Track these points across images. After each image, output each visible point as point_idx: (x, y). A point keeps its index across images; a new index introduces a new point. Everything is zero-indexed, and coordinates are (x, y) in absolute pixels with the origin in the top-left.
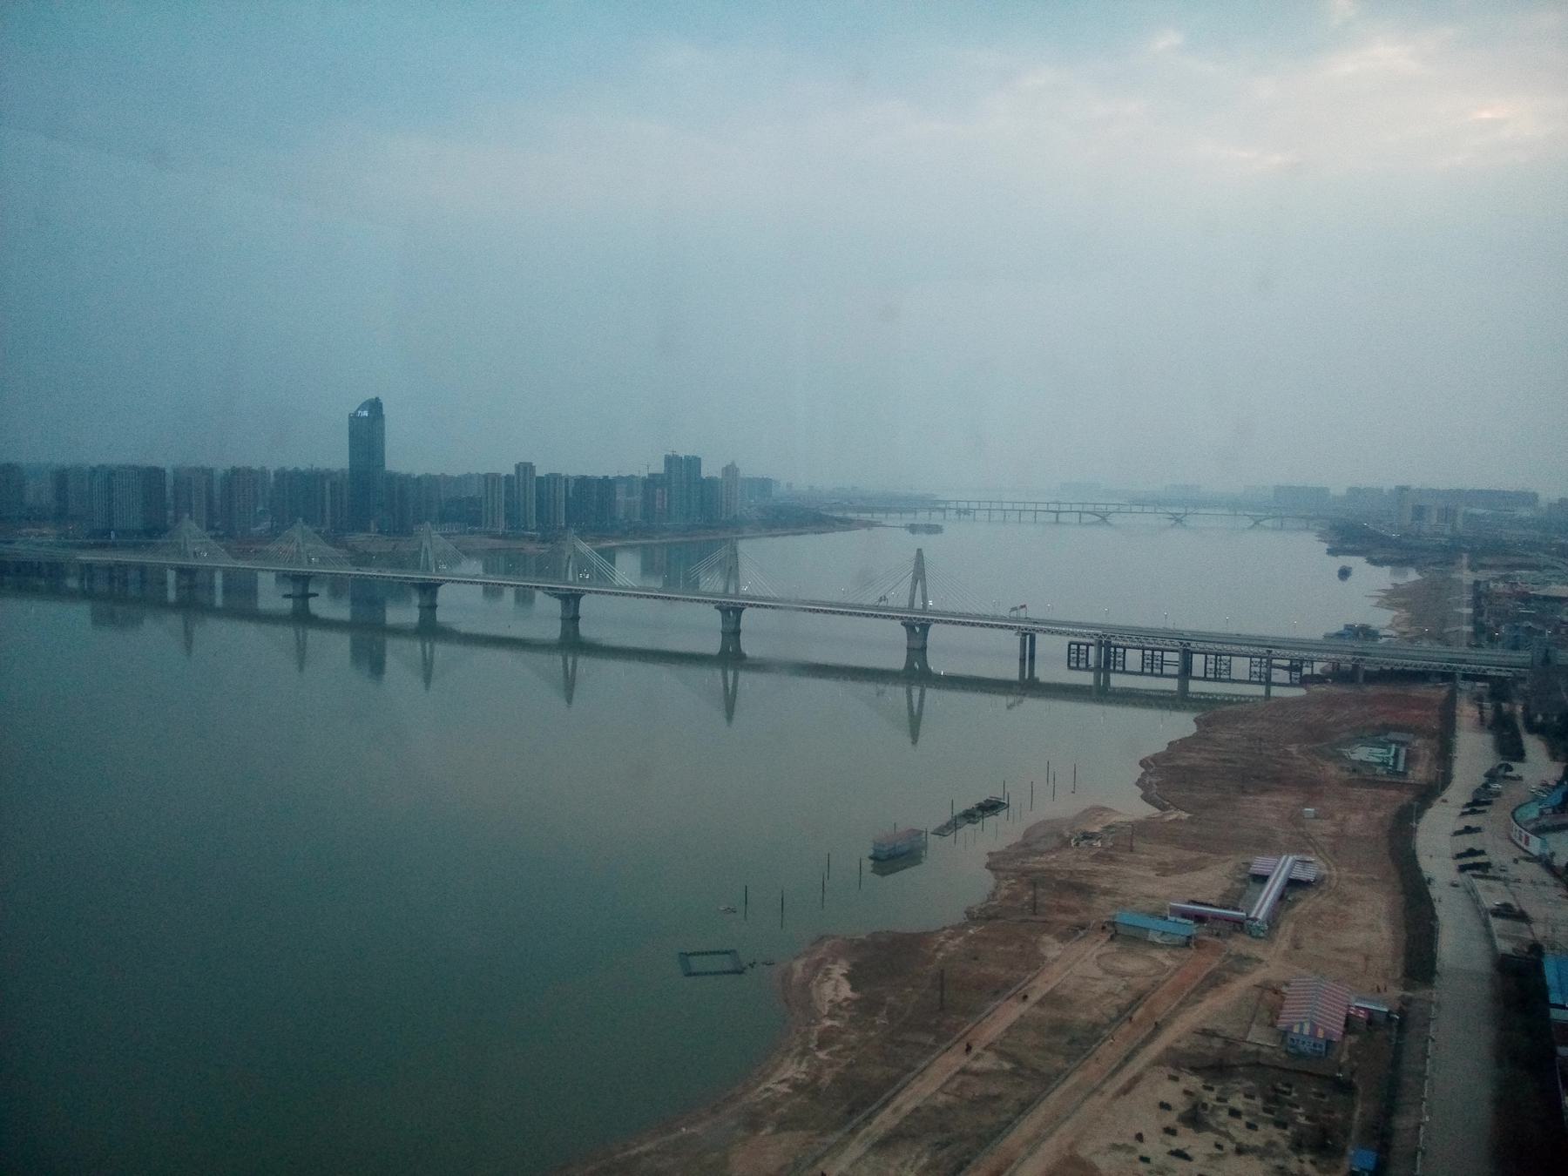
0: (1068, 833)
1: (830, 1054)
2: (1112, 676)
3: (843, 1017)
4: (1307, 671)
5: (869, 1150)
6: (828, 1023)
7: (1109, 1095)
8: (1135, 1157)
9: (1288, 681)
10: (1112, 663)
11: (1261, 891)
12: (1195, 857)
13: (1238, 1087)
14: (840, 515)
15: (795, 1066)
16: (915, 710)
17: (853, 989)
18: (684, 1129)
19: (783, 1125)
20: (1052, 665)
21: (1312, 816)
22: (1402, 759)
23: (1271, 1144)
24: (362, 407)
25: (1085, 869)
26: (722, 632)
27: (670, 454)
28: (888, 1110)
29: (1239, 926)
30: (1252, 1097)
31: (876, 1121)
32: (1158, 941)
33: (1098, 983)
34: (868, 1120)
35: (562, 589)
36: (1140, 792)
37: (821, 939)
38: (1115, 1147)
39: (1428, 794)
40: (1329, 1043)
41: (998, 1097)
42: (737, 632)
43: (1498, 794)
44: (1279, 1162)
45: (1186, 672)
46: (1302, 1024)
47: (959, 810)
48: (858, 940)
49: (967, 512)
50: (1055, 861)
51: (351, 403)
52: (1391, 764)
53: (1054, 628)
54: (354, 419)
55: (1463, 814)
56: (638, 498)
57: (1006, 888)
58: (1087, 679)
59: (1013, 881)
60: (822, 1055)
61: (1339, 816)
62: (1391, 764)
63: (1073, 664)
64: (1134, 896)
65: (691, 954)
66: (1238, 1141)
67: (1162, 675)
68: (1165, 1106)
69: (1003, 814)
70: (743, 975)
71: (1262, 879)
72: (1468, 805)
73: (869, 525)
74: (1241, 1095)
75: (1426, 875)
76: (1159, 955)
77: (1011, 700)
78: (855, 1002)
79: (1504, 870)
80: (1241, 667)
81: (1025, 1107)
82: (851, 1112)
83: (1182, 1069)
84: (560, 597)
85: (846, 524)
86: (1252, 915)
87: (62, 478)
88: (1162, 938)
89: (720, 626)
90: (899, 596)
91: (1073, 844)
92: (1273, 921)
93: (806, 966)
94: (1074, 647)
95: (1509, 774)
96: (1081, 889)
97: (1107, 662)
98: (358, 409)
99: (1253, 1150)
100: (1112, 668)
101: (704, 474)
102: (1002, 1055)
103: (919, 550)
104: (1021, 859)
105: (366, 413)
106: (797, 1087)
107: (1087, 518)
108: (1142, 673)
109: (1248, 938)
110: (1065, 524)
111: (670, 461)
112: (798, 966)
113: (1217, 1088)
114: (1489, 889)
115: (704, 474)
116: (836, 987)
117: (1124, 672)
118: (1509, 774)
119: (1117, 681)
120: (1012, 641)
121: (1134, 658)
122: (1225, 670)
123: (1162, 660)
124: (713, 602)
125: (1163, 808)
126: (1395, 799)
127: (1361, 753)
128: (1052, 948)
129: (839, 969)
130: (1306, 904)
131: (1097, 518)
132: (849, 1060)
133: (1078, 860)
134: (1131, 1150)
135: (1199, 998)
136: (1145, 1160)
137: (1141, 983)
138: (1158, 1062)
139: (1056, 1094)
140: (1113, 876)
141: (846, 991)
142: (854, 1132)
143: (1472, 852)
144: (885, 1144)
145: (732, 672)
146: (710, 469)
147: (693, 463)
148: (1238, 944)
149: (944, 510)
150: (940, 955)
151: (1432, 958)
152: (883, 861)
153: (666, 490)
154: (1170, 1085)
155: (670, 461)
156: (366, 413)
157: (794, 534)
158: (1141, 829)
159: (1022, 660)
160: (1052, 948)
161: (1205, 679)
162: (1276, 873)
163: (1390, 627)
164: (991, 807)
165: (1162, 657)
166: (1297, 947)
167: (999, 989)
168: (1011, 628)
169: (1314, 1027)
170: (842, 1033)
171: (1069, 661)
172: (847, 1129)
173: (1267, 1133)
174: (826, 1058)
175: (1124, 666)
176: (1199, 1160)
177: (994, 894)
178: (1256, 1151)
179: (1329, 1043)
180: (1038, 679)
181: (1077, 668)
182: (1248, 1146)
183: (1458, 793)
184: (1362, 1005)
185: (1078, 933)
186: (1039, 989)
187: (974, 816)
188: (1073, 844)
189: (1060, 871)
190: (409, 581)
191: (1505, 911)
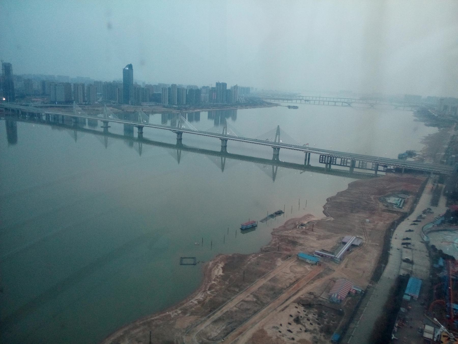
0: (298, 223)
1: (210, 292)
2: (332, 165)
3: (217, 281)
4: (389, 168)
5: (211, 323)
6: (213, 282)
7: (278, 311)
8: (277, 331)
9: (383, 170)
10: (332, 161)
11: (344, 246)
12: (330, 234)
13: (313, 311)
14: (268, 101)
15: (201, 295)
17: (223, 272)
18: (167, 313)
19: (192, 314)
20: (315, 161)
21: (368, 222)
22: (402, 203)
23: (315, 329)
24: (127, 67)
25: (298, 236)
26: (221, 146)
28: (220, 311)
29: (332, 259)
30: (315, 315)
31: (215, 314)
33: (288, 275)
34: (214, 314)
35: (177, 131)
36: (323, 209)
37: (219, 255)
38: (274, 327)
39: (404, 216)
40: (341, 301)
41: (248, 310)
42: (226, 146)
43: (424, 218)
44: (315, 335)
45: (353, 166)
46: (335, 294)
47: (270, 214)
48: (229, 256)
49: (308, 101)
50: (290, 233)
52: (398, 205)
54: (124, 70)
55: (412, 224)
56: (208, 95)
57: (274, 241)
58: (323, 166)
59: (277, 239)
60: (209, 292)
61: (376, 222)
62: (398, 205)
63: (321, 161)
64: (308, 246)
65: (184, 258)
66: (306, 328)
67: (346, 166)
68: (291, 316)
69: (282, 215)
70: (195, 266)
71: (344, 243)
72: (414, 221)
73: (277, 105)
74: (312, 314)
75: (392, 245)
76: (307, 267)
77: (302, 171)
78: (222, 276)
79: (414, 246)
80: (370, 165)
81: (255, 312)
82: (210, 311)
83: (300, 305)
84: (177, 133)
85: (270, 105)
86: (336, 257)
87: (43, 84)
88: (310, 262)
89: (221, 145)
91: (298, 227)
92: (341, 259)
93: (212, 264)
94: (322, 156)
95: (430, 211)
96: (294, 243)
97: (330, 162)
98: (126, 67)
99: (310, 331)
100: (332, 163)
102: (255, 296)
103: (278, 126)
104: (281, 232)
105: (128, 69)
106: (199, 302)
107: (344, 104)
108: (341, 165)
109: (334, 263)
110: (337, 106)
111: (218, 84)
112: (211, 263)
113: (307, 311)
114: (407, 252)
116: (218, 272)
117: (335, 164)
118: (430, 211)
119: (333, 167)
120: (303, 154)
121: (338, 161)
122: (365, 166)
123: (347, 162)
124: (219, 138)
125: (327, 216)
126: (396, 217)
127: (392, 200)
128: (279, 262)
129: (221, 265)
130: (355, 252)
131: (347, 104)
132: (215, 295)
133: (297, 233)
134: (278, 328)
135: (313, 282)
136: (280, 332)
137: (299, 276)
138: (294, 302)
139: (265, 309)
140: (304, 239)
141: (221, 273)
142: (209, 317)
143: (407, 239)
144: (215, 322)
147: (224, 85)
148: (330, 265)
149: (301, 100)
150: (249, 263)
151: (381, 274)
152: (243, 230)
153: (216, 93)
154: (295, 309)
155: (218, 84)
156: (128, 69)
157: (253, 108)
158: (319, 223)
159: (306, 160)
160: (279, 262)
161: (359, 168)
162: (349, 242)
163: (421, 151)
164: (279, 213)
165: (347, 161)
166: (346, 267)
167: (262, 275)
168: (303, 151)
169: (338, 295)
170: (216, 286)
171: (320, 161)
172: (207, 316)
173: (316, 326)
174: (209, 293)
175: (336, 163)
176: (295, 332)
177: (270, 243)
178: (310, 331)
179: (341, 301)
180: (310, 165)
181: (322, 163)
182: (308, 329)
183: (413, 217)
184: (354, 289)
185: (288, 258)
186: (272, 275)
187: (273, 216)
188: (298, 227)
189: (290, 236)
191: (407, 261)
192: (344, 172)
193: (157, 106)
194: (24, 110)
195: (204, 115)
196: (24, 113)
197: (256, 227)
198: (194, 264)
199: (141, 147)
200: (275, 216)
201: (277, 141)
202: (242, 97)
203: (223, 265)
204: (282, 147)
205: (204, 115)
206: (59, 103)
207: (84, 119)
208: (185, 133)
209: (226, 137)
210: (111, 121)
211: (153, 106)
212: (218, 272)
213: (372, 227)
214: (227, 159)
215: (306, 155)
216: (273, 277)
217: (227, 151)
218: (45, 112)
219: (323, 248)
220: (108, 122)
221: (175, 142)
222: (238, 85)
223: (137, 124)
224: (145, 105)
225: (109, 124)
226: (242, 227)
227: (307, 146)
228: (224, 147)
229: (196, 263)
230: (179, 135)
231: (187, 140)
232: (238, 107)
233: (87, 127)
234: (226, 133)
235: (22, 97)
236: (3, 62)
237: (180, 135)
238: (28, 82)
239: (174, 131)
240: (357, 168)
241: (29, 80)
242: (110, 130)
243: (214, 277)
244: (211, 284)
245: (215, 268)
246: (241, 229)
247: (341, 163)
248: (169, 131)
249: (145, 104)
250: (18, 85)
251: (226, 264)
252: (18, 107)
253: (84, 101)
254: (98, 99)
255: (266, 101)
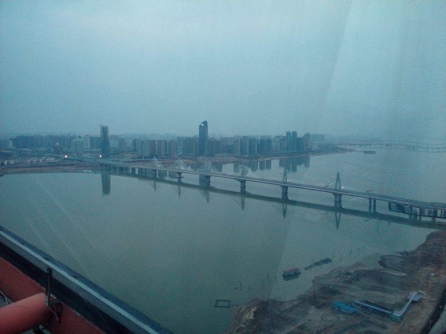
6: (242, 325)
16: (285, 208)
17: (254, 316)
24: (202, 123)
27: (288, 131)
32: (344, 311)
35: (241, 179)
42: (340, 201)
45: (435, 216)
49: (389, 145)
51: (200, 122)
53: (383, 197)
54: (200, 126)
76: (341, 316)
77: (366, 218)
84: (240, 181)
85: (344, 150)
87: (135, 142)
90: (332, 185)
103: (338, 173)
105: (203, 125)
111: (288, 133)
112: (244, 307)
120: (280, 189)
133: (339, 282)
141: (251, 317)
145: (285, 205)
146: (300, 134)
147: (295, 133)
156: (203, 125)
159: (370, 207)
161: (441, 217)
164: (327, 261)
170: (244, 329)
190: (203, 175)
192: (442, 223)
193: (229, 156)
194: (115, 165)
195: (275, 163)
196: (115, 168)
197: (299, 275)
198: (228, 307)
199: (340, 219)
200: (321, 264)
201: (338, 188)
202: (316, 144)
203: (256, 309)
204: (289, 186)
205: (275, 163)
206: (145, 158)
207: (166, 172)
208: (248, 181)
209: (286, 184)
210: (183, 172)
211: (225, 156)
212: (249, 316)
213: (437, 281)
214: (288, 205)
215: (370, 202)
216: (302, 324)
217: (288, 197)
218: (131, 166)
219: (367, 299)
220: (181, 173)
221: (239, 190)
222: (310, 134)
223: (205, 174)
224: (218, 156)
225: (183, 175)
226: (284, 273)
227: (371, 192)
228: (285, 194)
229: (230, 306)
230: (242, 182)
231: (250, 188)
232: (309, 155)
233: (167, 178)
234: (286, 180)
235: (117, 153)
236: (102, 126)
237: (243, 183)
238: (122, 141)
239: (237, 180)
240: (439, 217)
241: (123, 139)
242: (183, 180)
243: (243, 321)
244: (239, 327)
245: (247, 312)
246: (283, 276)
247: (441, 215)
248: (233, 179)
249: (218, 155)
250: (113, 144)
251: (258, 309)
252: (111, 162)
253: (165, 155)
254: (179, 153)
255: (340, 146)
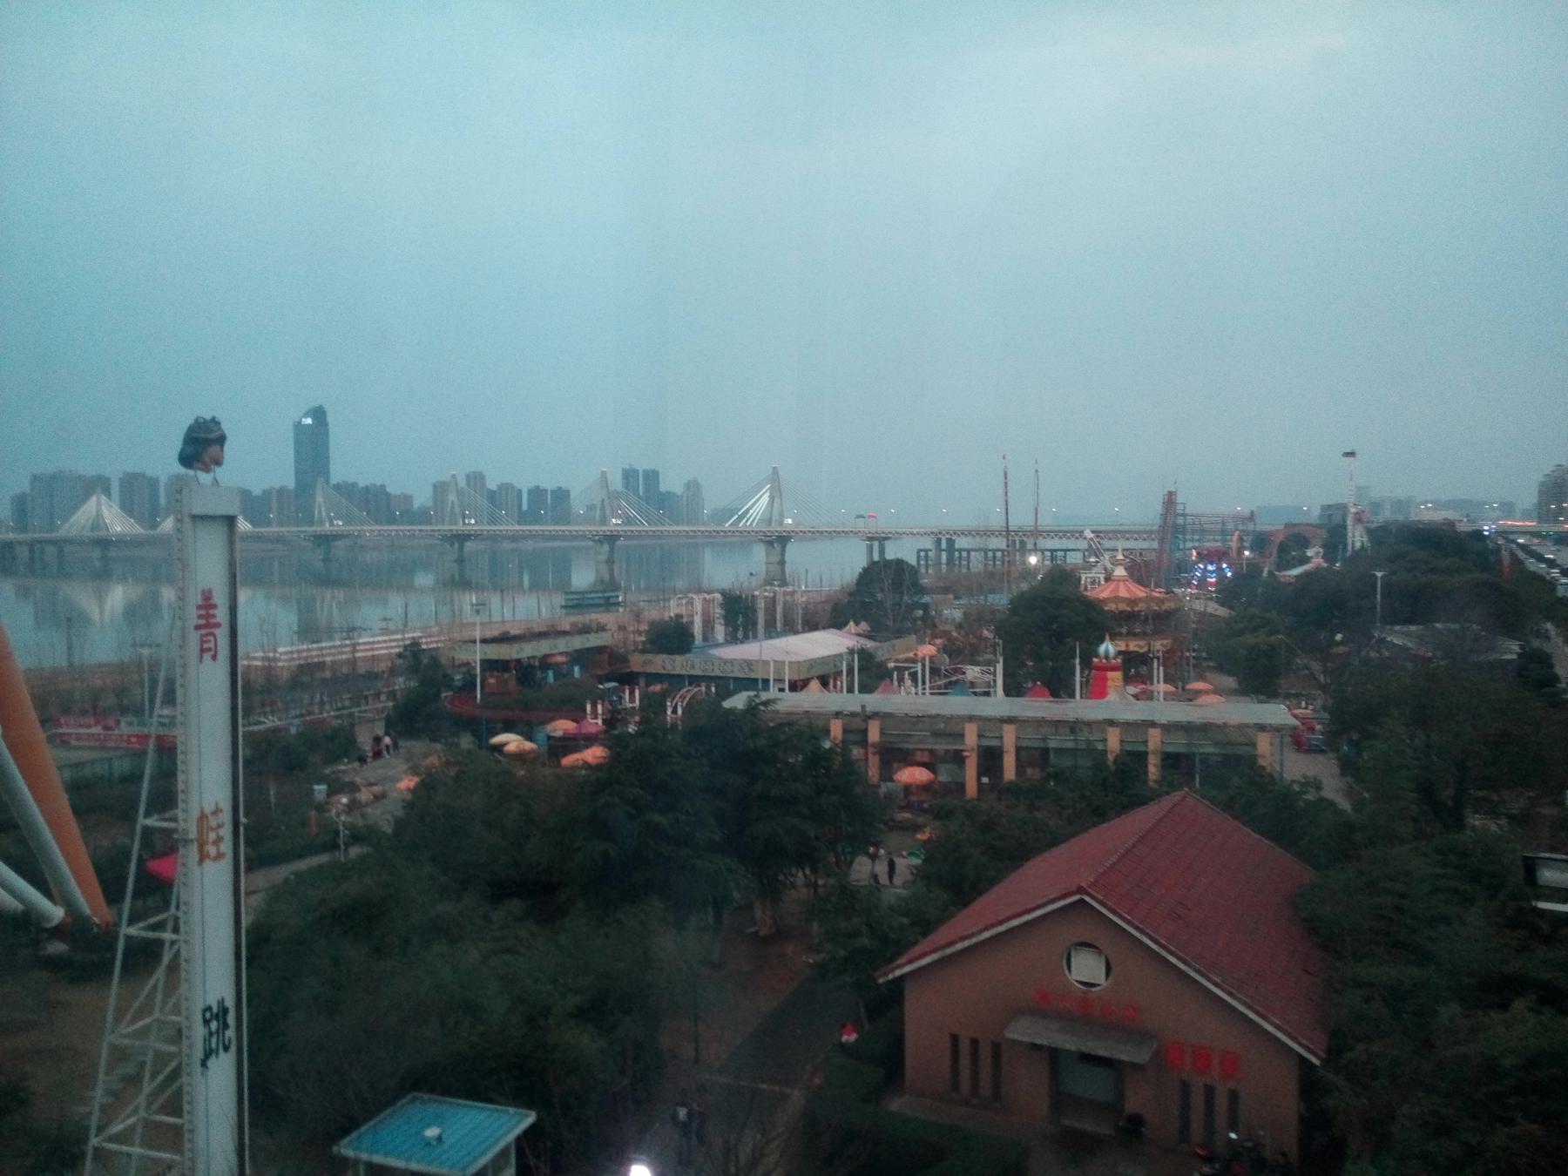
27: (628, 467)
101: (663, 488)
105: (309, 421)
115: (663, 488)
156: (309, 421)
